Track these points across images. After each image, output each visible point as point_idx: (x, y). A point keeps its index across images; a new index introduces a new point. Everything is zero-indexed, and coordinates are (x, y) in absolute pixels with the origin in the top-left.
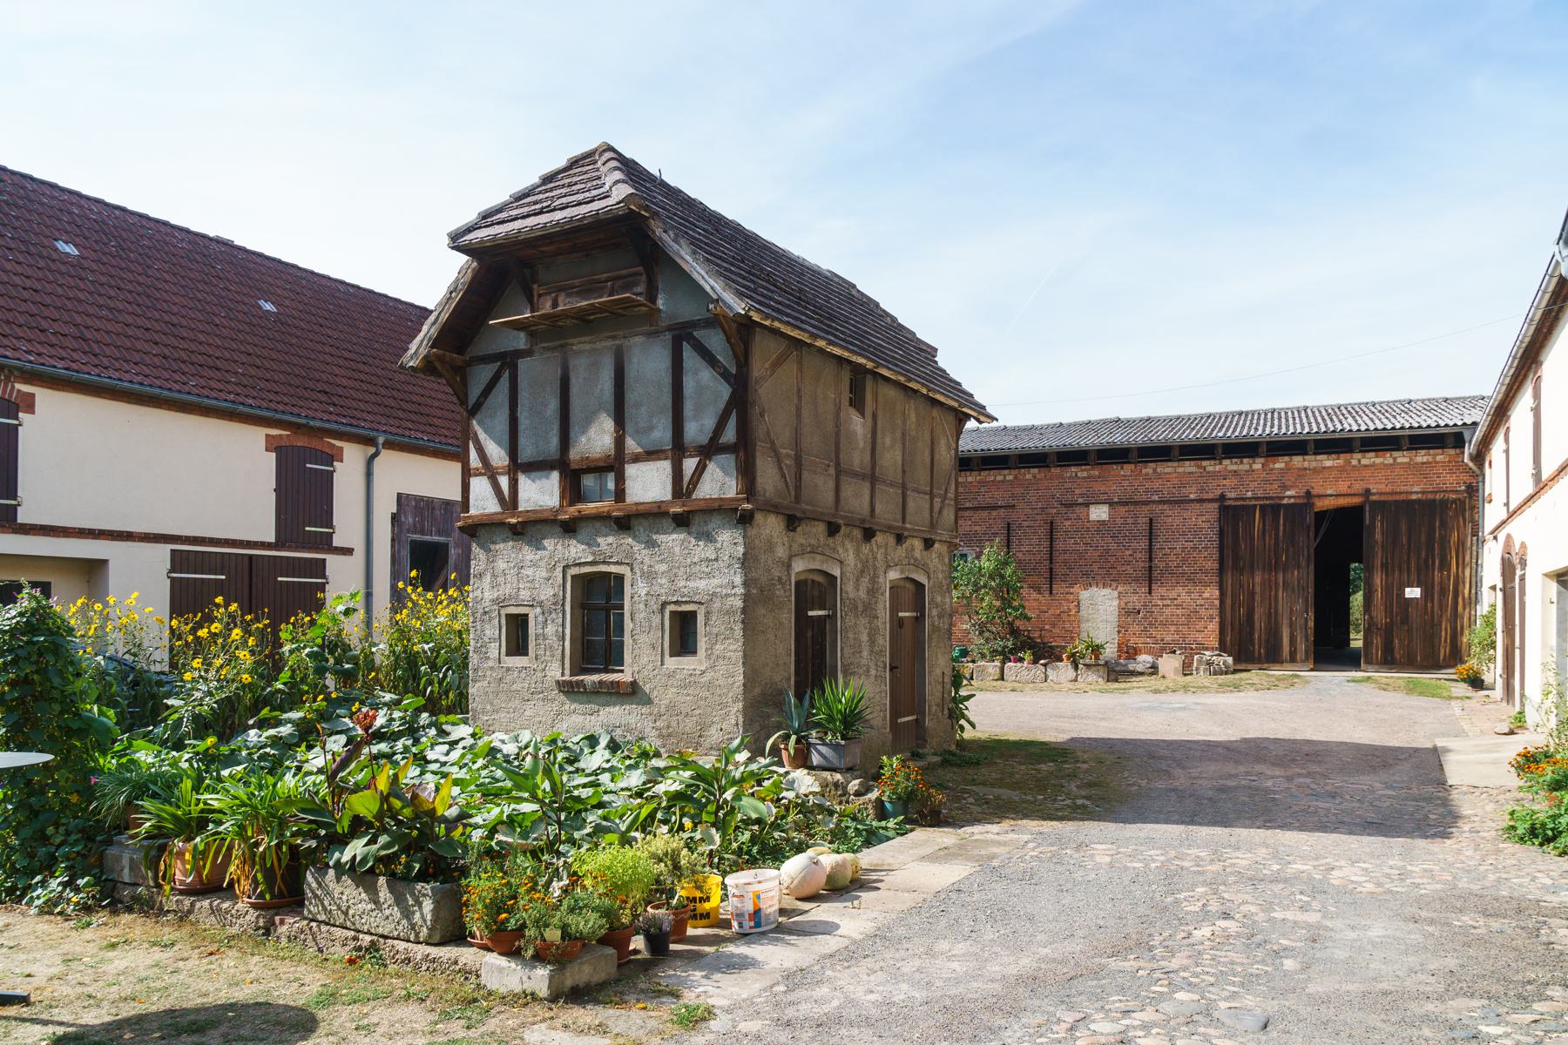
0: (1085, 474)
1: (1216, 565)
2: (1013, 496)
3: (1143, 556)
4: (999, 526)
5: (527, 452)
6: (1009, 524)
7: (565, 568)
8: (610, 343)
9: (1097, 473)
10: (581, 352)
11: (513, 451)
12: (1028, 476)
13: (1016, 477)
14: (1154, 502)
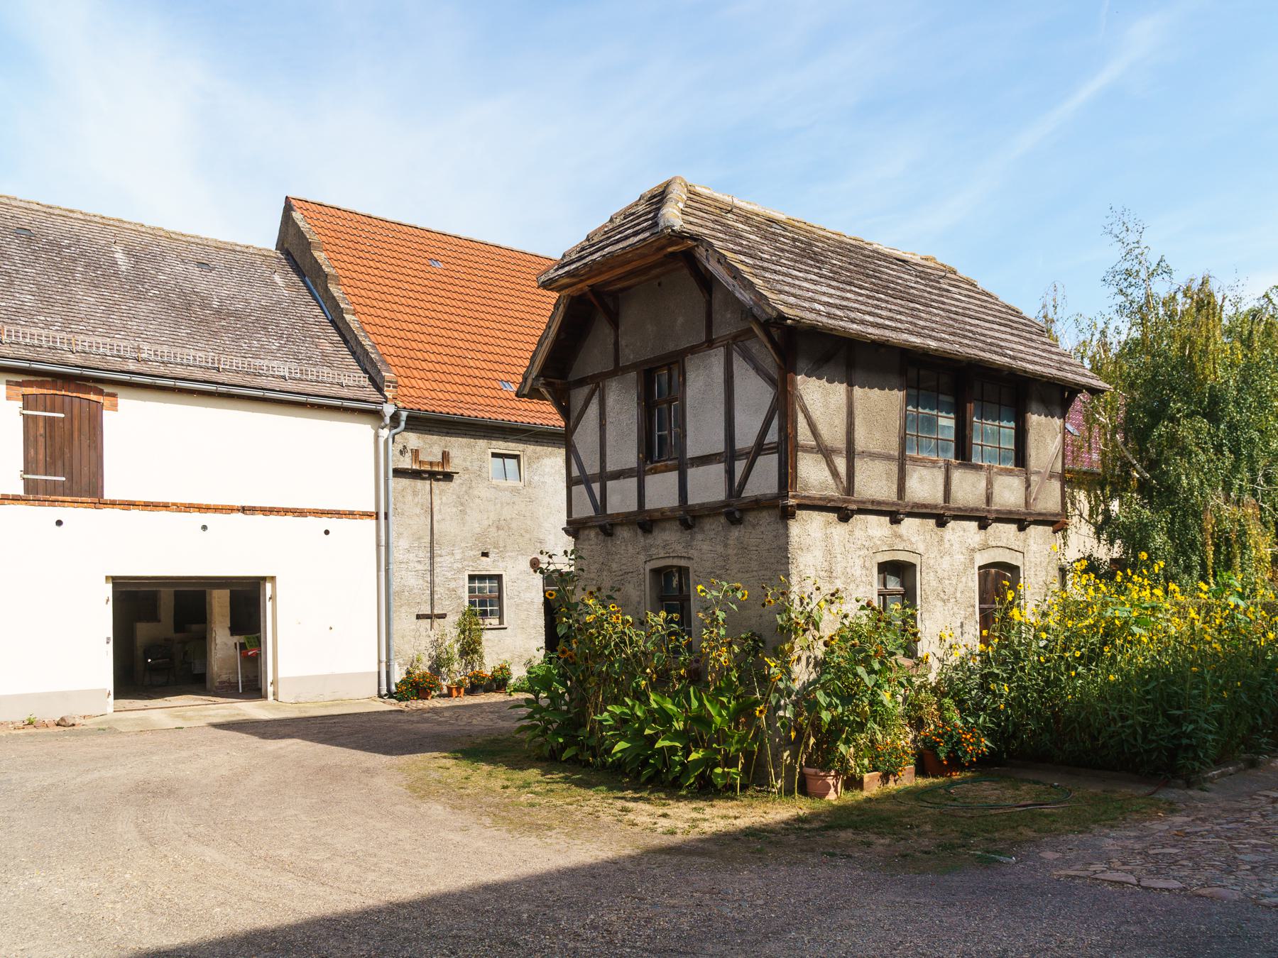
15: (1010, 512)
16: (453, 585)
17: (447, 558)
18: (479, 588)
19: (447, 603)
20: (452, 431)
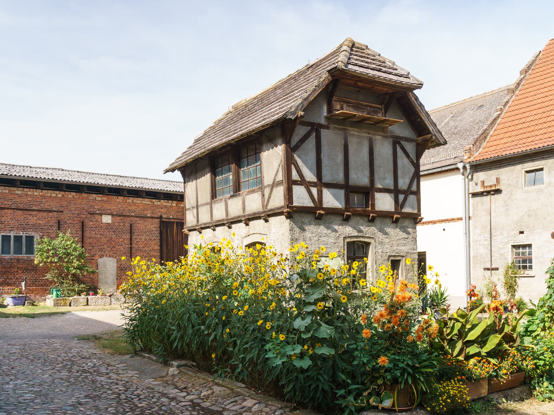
0: (100, 199)
1: (159, 248)
2: (62, 206)
3: (127, 242)
4: (53, 222)
5: (327, 178)
6: (59, 221)
7: (345, 238)
8: (367, 135)
9: (106, 199)
10: (353, 135)
11: (319, 175)
12: (70, 196)
13: (63, 196)
14: (132, 216)
15: (255, 214)
16: (502, 251)
17: (499, 236)
18: (522, 252)
19: (500, 261)
20: (502, 165)
